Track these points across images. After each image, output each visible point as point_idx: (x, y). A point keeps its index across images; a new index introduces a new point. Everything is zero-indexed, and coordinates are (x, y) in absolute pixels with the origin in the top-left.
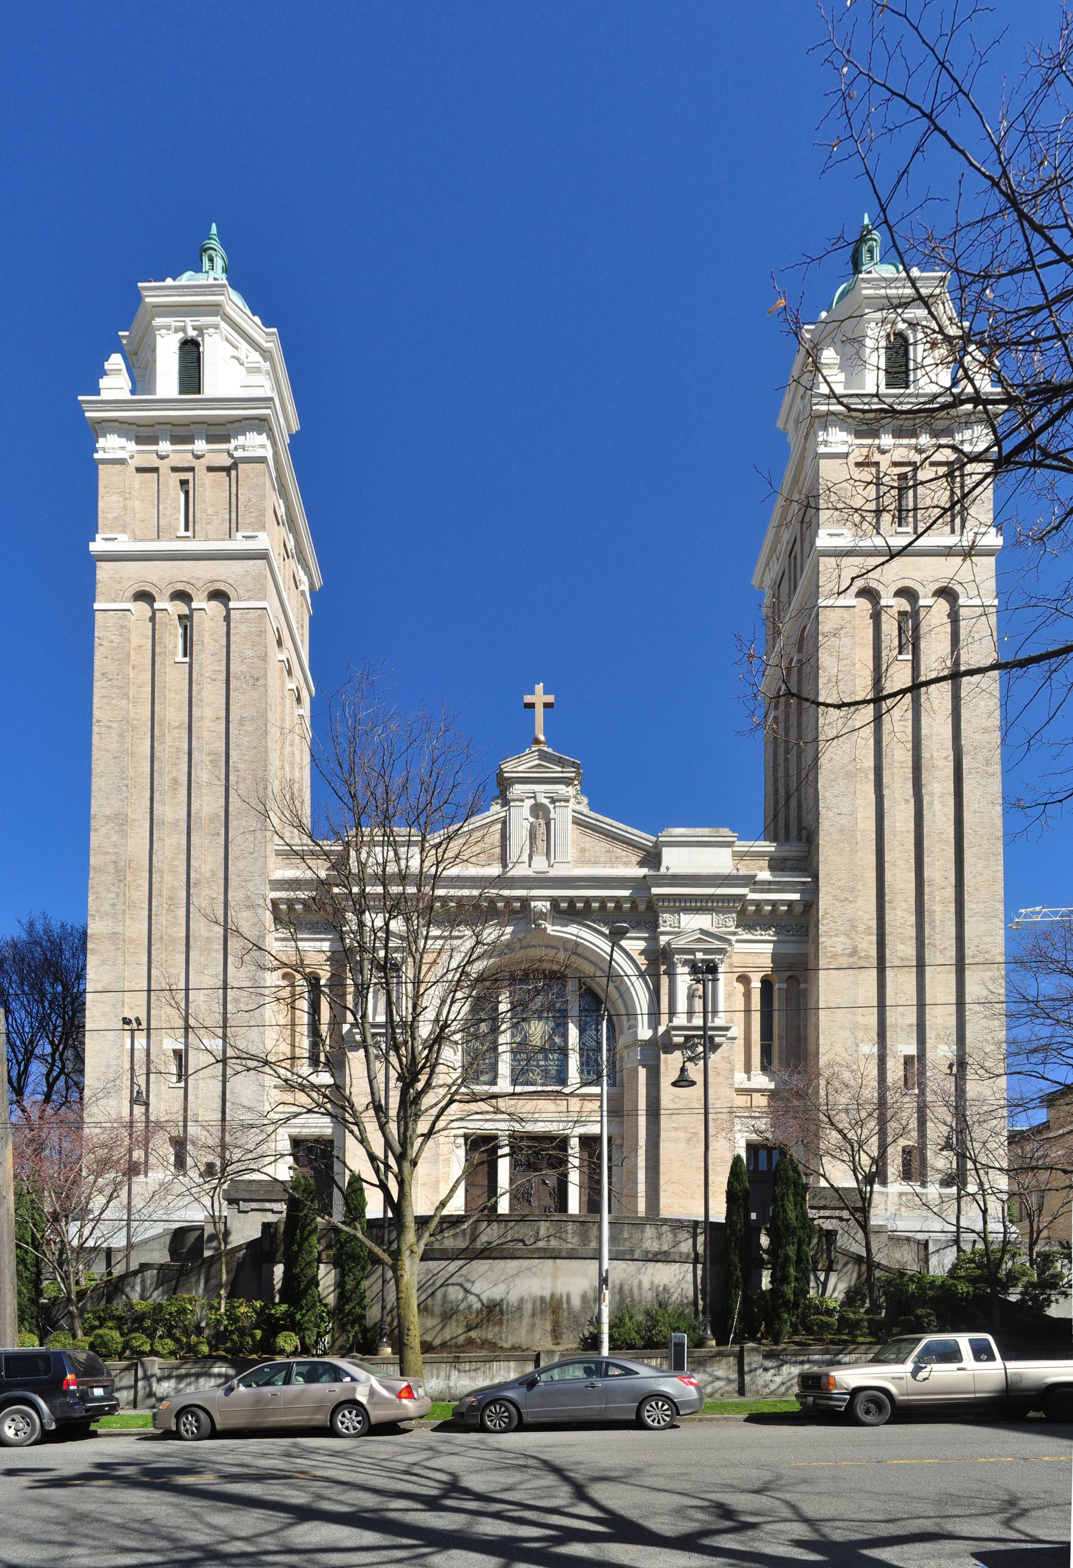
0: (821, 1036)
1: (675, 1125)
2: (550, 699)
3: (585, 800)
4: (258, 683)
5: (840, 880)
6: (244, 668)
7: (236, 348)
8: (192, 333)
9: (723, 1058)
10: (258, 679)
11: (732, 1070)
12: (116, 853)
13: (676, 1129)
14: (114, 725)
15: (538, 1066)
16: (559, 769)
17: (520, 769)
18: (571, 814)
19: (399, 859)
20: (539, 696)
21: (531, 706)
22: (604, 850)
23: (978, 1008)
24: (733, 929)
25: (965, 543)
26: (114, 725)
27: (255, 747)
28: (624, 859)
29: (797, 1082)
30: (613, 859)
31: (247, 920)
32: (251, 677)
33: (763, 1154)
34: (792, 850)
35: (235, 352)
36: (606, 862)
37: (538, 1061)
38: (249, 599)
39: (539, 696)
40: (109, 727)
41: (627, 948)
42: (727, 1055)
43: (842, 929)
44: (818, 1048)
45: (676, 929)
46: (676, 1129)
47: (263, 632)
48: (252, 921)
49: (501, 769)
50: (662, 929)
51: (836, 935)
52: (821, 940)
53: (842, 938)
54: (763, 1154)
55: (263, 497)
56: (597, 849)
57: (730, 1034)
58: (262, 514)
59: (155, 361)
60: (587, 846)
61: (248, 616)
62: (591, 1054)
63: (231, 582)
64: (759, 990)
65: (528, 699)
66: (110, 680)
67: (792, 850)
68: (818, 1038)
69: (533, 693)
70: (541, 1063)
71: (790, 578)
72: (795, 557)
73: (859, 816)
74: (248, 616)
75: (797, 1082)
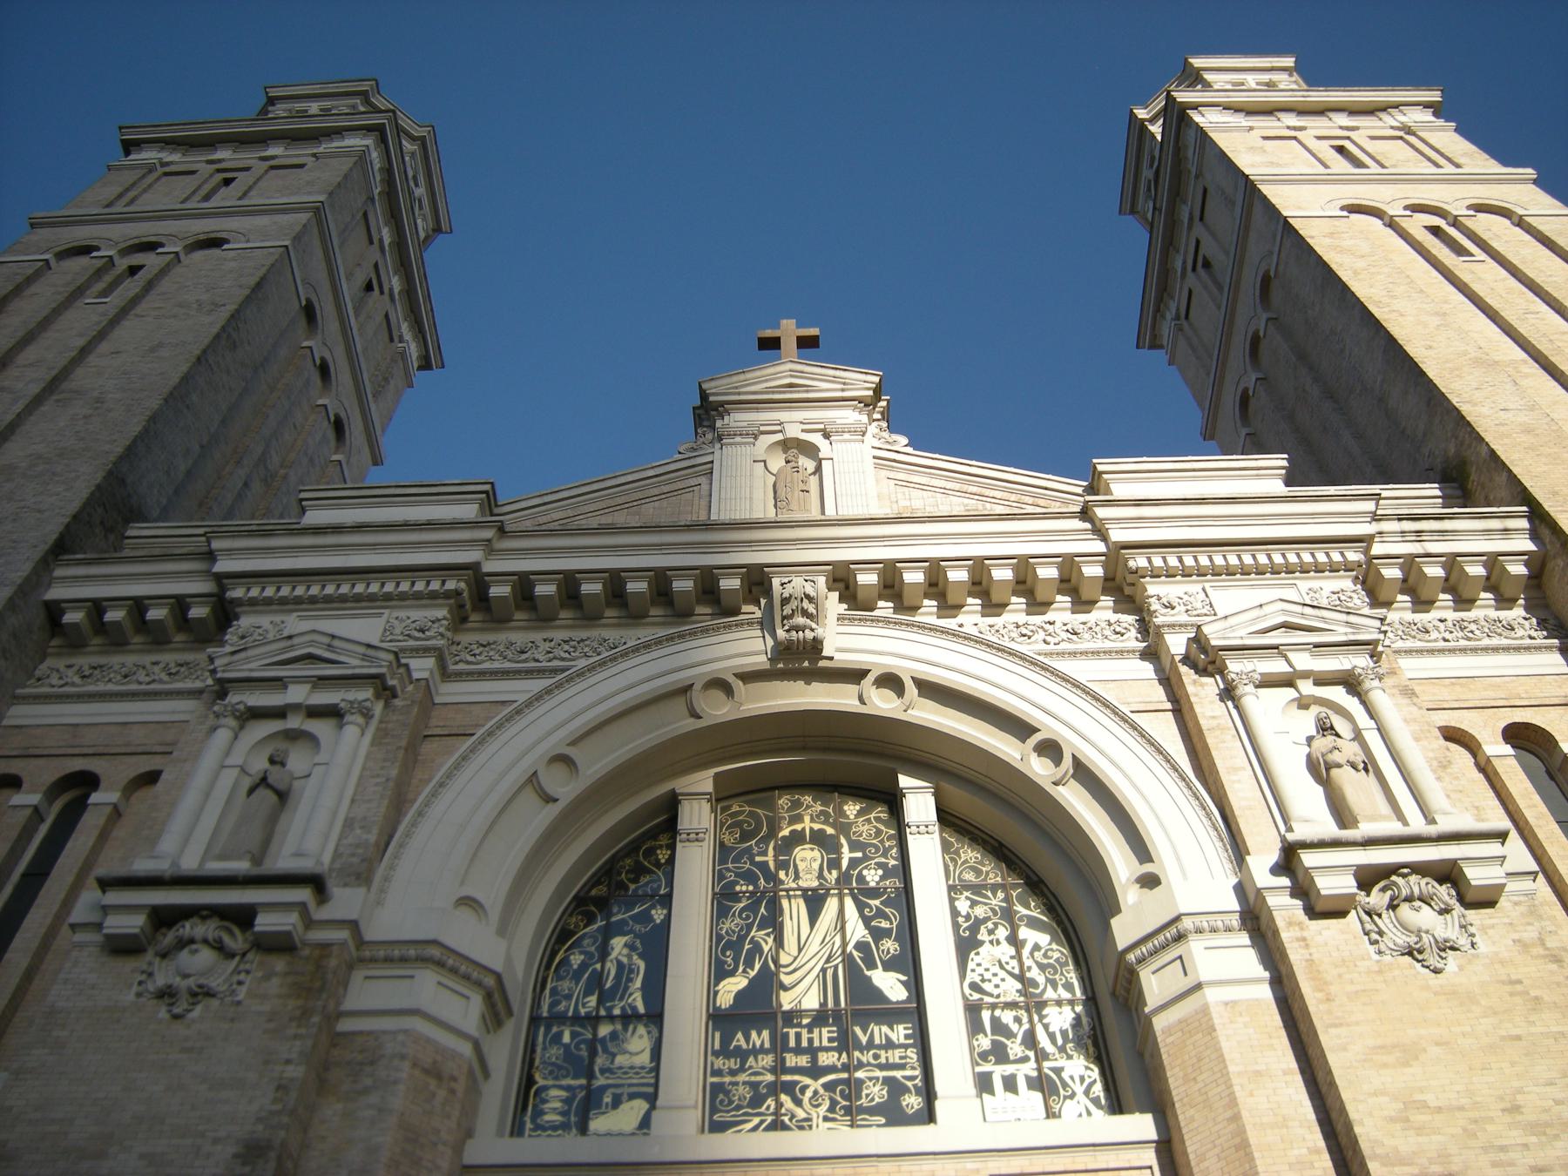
9: (1523, 945)
15: (815, 1071)
37: (813, 1051)
42: (1530, 934)
62: (1007, 1017)
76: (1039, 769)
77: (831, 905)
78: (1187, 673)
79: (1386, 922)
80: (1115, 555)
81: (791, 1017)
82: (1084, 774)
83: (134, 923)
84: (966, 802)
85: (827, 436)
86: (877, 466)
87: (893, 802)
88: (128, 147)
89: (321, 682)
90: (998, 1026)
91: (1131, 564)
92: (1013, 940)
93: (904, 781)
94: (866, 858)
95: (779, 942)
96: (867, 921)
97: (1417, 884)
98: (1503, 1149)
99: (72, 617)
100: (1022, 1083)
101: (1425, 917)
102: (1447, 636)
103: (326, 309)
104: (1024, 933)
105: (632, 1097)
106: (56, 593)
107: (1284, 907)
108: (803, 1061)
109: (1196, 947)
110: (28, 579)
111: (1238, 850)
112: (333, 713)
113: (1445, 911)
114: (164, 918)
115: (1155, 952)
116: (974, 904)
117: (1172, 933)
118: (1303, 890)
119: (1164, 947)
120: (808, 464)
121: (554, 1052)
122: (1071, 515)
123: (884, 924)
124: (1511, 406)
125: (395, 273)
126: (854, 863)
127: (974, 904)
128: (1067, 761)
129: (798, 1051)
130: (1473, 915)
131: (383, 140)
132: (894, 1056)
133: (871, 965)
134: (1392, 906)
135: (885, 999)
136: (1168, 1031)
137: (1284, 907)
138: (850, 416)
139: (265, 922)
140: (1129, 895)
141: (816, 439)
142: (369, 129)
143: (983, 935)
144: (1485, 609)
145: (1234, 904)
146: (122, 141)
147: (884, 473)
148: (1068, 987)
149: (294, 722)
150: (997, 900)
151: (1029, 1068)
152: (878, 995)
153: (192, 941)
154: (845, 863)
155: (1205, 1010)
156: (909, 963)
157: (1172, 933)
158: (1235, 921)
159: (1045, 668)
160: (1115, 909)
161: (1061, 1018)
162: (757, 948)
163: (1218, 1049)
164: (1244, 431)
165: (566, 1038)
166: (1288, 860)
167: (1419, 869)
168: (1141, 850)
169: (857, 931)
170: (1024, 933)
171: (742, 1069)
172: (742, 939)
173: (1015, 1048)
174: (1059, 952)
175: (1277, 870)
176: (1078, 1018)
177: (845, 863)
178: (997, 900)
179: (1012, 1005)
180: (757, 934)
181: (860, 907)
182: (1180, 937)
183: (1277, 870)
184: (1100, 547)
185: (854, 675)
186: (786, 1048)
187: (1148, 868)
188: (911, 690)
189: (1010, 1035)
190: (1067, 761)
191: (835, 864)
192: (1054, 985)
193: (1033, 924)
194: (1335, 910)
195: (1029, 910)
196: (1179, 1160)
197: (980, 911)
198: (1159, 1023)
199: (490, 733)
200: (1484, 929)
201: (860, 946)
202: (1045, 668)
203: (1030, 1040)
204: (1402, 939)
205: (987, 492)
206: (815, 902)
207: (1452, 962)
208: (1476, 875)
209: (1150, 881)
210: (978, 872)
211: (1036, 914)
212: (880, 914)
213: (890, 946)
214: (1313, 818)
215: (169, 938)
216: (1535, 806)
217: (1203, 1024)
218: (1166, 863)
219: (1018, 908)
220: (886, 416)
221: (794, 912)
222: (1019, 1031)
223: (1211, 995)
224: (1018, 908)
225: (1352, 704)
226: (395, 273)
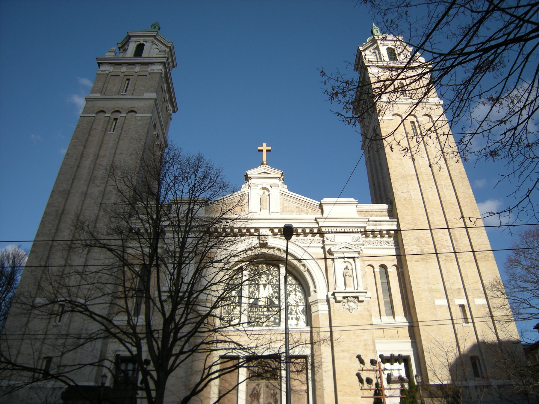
0: (414, 296)
1: (342, 349)
2: (270, 148)
3: (286, 186)
4: (142, 141)
5: (408, 220)
6: (137, 136)
7: (158, 46)
8: (142, 42)
9: (365, 309)
11: (371, 316)
13: (343, 351)
17: (255, 174)
19: (252, 250)
20: (264, 147)
21: (262, 151)
23: (480, 319)
28: (306, 211)
30: (300, 211)
32: (139, 139)
34: (398, 247)
36: (296, 212)
37: (263, 312)
38: (144, 113)
39: (264, 147)
40: (72, 156)
42: (366, 307)
43: (414, 242)
44: (414, 302)
45: (334, 243)
46: (343, 351)
49: (247, 174)
51: (412, 245)
52: (405, 247)
53: (415, 246)
57: (367, 295)
60: (287, 205)
64: (379, 272)
65: (259, 148)
66: (78, 140)
67: (398, 247)
68: (413, 297)
69: (262, 146)
70: (266, 313)
73: (411, 193)
76: (302, 268)
77: (267, 286)
78: (327, 253)
79: (346, 304)
80: (319, 229)
81: (261, 306)
82: (308, 270)
84: (290, 269)
85: (271, 187)
86: (280, 195)
87: (279, 268)
88: (100, 64)
90: (291, 309)
91: (322, 230)
92: (295, 294)
93: (281, 265)
94: (274, 278)
95: (259, 293)
96: (273, 290)
97: (351, 299)
98: (351, 338)
100: (294, 318)
101: (352, 304)
102: (377, 244)
103: (158, 125)
104: (298, 293)
105: (237, 318)
107: (332, 300)
108: (262, 313)
109: (319, 304)
111: (328, 291)
113: (355, 303)
115: (314, 304)
116: (290, 287)
117: (316, 302)
118: (335, 298)
119: (315, 303)
120: (267, 193)
121: (225, 311)
122: (313, 220)
123: (276, 290)
124: (404, 192)
126: (271, 279)
127: (290, 287)
128: (306, 268)
129: (262, 312)
130: (359, 303)
131: (165, 65)
133: (273, 298)
134: (347, 302)
135: (275, 304)
136: (314, 316)
137: (332, 300)
138: (276, 181)
140: (312, 293)
141: (269, 187)
142: (161, 63)
143: (291, 293)
144: (386, 239)
145: (326, 298)
146: (98, 63)
147: (282, 197)
148: (303, 303)
150: (294, 287)
151: (295, 316)
152: (273, 303)
154: (270, 279)
155: (318, 314)
156: (278, 298)
157: (316, 302)
158: (326, 301)
160: (310, 296)
161: (301, 308)
162: (255, 294)
163: (319, 320)
164: (368, 155)
165: (227, 309)
166: (334, 294)
168: (315, 287)
169: (271, 292)
170: (298, 293)
171: (253, 314)
172: (253, 292)
173: (293, 313)
174: (302, 297)
175: (332, 295)
176: (303, 309)
177: (270, 279)
178: (294, 287)
179: (294, 306)
180: (256, 291)
181: (272, 287)
182: (317, 303)
183: (332, 295)
184: (317, 226)
185: (273, 248)
186: (259, 311)
187: (315, 289)
188: (282, 251)
189: (293, 311)
190: (306, 268)
191: (268, 279)
192: (301, 302)
193: (299, 291)
194: (340, 302)
195: (299, 289)
197: (291, 289)
198: (313, 315)
200: (360, 306)
201: (272, 294)
203: (296, 312)
204: (348, 307)
205: (301, 203)
206: (265, 285)
208: (360, 299)
209: (315, 292)
210: (291, 281)
211: (300, 290)
212: (275, 289)
213: (276, 294)
214: (341, 287)
216: (438, 208)
217: (318, 316)
218: (318, 290)
219: (297, 288)
220: (283, 180)
221: (261, 287)
222: (294, 310)
223: (320, 312)
224: (297, 288)
225: (352, 262)
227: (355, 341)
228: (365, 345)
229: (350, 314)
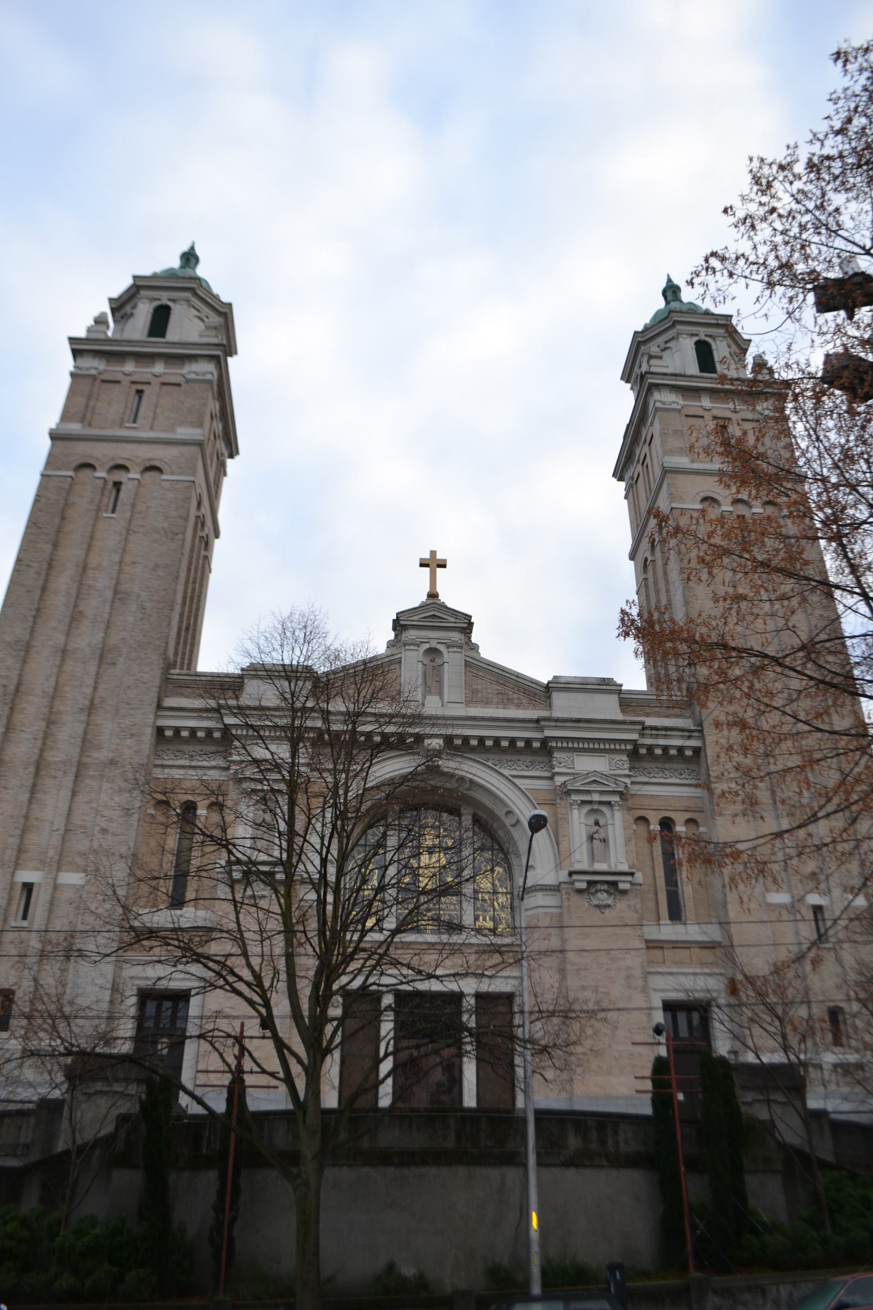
4: (177, 537)
6: (165, 525)
8: (165, 302)
10: (177, 534)
12: (7, 676)
14: (33, 564)
16: (453, 620)
18: (464, 658)
22: (495, 692)
24: (627, 772)
25: (48, 967)
26: (33, 564)
27: (165, 590)
29: (673, 888)
31: (129, 748)
33: (682, 1017)
35: (197, 314)
36: (498, 703)
41: (522, 787)
47: (188, 499)
48: (135, 749)
50: (557, 770)
54: (682, 1017)
55: (205, 405)
56: (489, 691)
58: (202, 415)
59: (518, 675)
61: (177, 487)
63: (166, 460)
71: (645, 480)
72: (647, 466)
74: (177, 487)
75: (673, 888)
83: (584, 885)
86: (466, 665)
89: (602, 793)
97: (606, 887)
99: (169, 733)
106: (161, 723)
110: (655, 716)
112: (608, 804)
114: (590, 883)
125: (700, 402)
132: (452, 907)
139: (621, 886)
149: (596, 807)
153: (600, 890)
159: (510, 780)
167: (607, 882)
196: (194, 656)
199: (384, 760)
202: (510, 780)
207: (607, 911)
215: (593, 890)
226: (700, 402)
227: (608, 970)
228: (628, 977)
229: (601, 915)
